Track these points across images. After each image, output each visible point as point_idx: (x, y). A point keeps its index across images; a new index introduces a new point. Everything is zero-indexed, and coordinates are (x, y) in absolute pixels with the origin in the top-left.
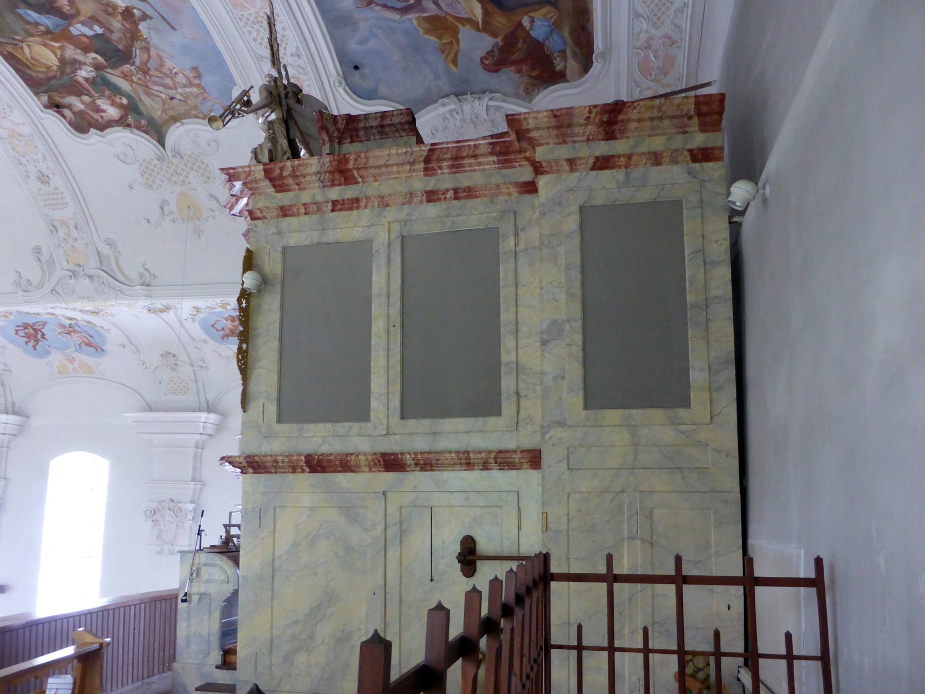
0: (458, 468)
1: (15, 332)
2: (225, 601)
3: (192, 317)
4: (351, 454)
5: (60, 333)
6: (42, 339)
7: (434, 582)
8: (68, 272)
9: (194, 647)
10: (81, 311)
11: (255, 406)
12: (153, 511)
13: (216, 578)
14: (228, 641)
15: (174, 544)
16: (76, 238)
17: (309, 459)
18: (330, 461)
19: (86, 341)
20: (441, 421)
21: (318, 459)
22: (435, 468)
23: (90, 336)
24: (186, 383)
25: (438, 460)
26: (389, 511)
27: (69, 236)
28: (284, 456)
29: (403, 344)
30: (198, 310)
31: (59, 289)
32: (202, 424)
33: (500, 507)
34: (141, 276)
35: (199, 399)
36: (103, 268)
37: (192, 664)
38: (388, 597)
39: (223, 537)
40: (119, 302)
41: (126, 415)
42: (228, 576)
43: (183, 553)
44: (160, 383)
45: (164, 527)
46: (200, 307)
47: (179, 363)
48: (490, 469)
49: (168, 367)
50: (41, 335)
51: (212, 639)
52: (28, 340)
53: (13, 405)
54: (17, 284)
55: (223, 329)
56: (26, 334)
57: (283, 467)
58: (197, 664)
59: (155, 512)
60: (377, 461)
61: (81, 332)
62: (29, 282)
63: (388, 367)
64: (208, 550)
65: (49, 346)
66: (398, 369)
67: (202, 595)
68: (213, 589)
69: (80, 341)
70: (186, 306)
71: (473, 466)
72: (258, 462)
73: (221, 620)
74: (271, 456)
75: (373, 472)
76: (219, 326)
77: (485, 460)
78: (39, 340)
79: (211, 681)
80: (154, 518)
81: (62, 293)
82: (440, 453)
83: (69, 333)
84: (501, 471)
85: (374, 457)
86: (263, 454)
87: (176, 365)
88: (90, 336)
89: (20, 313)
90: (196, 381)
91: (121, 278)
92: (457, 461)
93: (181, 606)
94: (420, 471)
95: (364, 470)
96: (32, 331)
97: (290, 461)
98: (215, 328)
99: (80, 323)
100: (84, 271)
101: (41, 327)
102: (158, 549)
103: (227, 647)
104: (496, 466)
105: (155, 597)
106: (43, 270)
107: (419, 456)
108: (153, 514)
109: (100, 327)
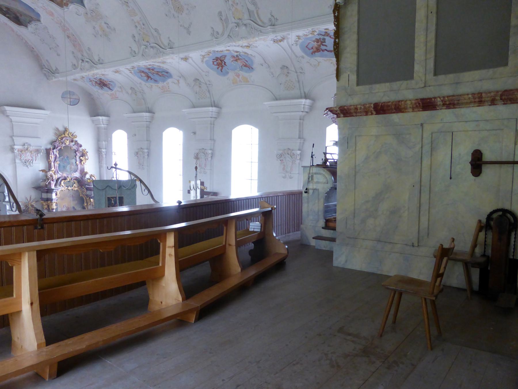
0: (473, 105)
1: (212, 63)
2: (326, 193)
3: (296, 42)
4: (402, 101)
5: (232, 61)
6: (224, 66)
7: (452, 180)
8: (235, 24)
9: (311, 217)
10: (241, 46)
11: (344, 77)
12: (280, 155)
13: (321, 181)
14: (328, 215)
15: (291, 173)
16: (237, 3)
17: (376, 105)
18: (388, 106)
19: (244, 64)
20: (462, 75)
21: (381, 104)
22: (456, 107)
23: (246, 61)
24: (294, 83)
25: (459, 100)
26: (424, 136)
27: (234, 3)
28: (361, 105)
29: (437, 24)
30: (299, 37)
31: (231, 35)
32: (303, 106)
33: (502, 130)
34: (270, 20)
35: (301, 92)
36: (251, 19)
37: (310, 226)
38: (422, 188)
39: (324, 160)
40: (260, 38)
41: (265, 103)
42: (327, 180)
43: (304, 167)
44: (281, 84)
45: (286, 164)
46: (300, 35)
47: (290, 72)
48: (496, 105)
49: (284, 74)
50: (224, 63)
51: (320, 213)
52: (218, 67)
53: (214, 102)
54: (212, 35)
55: (312, 48)
56: (217, 63)
57: (361, 112)
58: (313, 226)
59: (281, 156)
60: (418, 104)
61: (242, 59)
62: (218, 33)
63: (426, 42)
64: (316, 166)
65: (228, 69)
66: (433, 42)
67: (314, 190)
68: (320, 187)
69: (242, 65)
70: (293, 36)
71: (484, 103)
72: (346, 110)
73: (324, 204)
74: (354, 106)
75: (416, 111)
76: (310, 46)
77: (493, 98)
78: (223, 66)
79: (319, 235)
80: (281, 159)
81: (232, 36)
82: (461, 95)
83: (236, 60)
84: (504, 105)
85: (416, 101)
86: (349, 105)
87: (288, 73)
88: (246, 61)
89: (214, 51)
90: (299, 82)
91: (260, 23)
92: (473, 100)
93: (305, 195)
94: (446, 109)
95: (409, 111)
96: (220, 61)
97: (365, 108)
98: (308, 48)
99: (242, 54)
100: (242, 22)
101: (223, 59)
102: (284, 175)
103: (328, 218)
104: (501, 102)
105: (290, 193)
106: (223, 24)
107: (446, 99)
108: (280, 156)
109: (250, 55)
